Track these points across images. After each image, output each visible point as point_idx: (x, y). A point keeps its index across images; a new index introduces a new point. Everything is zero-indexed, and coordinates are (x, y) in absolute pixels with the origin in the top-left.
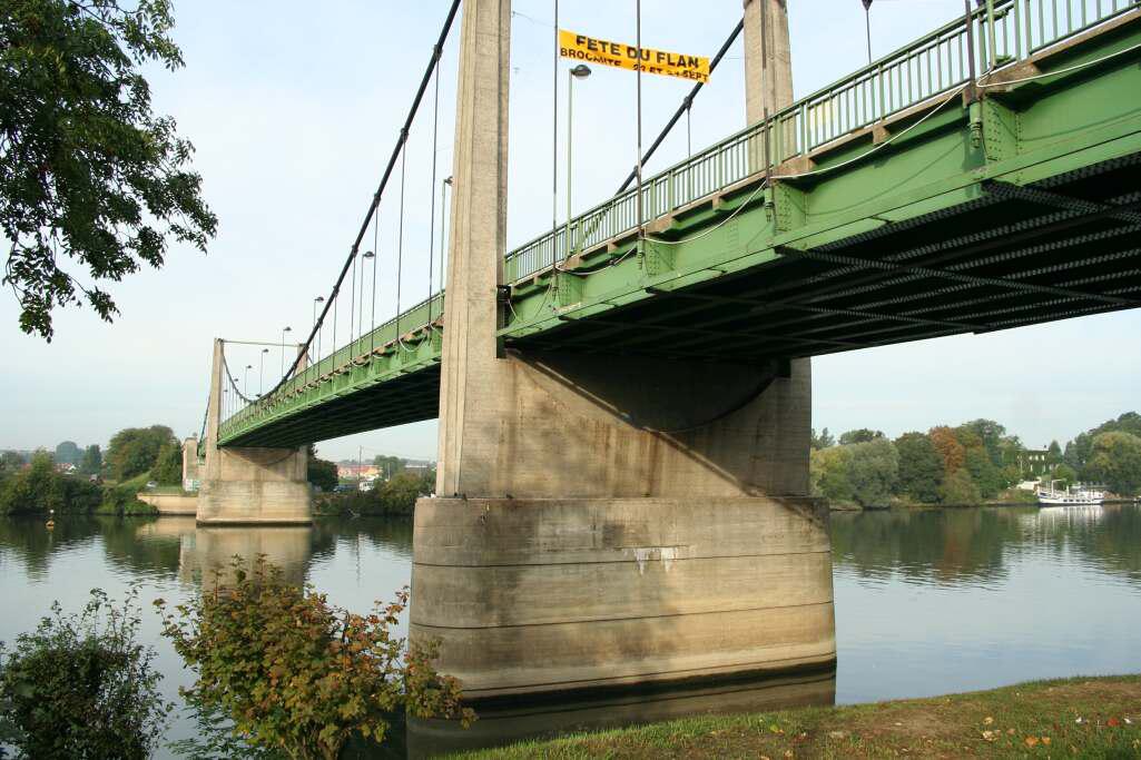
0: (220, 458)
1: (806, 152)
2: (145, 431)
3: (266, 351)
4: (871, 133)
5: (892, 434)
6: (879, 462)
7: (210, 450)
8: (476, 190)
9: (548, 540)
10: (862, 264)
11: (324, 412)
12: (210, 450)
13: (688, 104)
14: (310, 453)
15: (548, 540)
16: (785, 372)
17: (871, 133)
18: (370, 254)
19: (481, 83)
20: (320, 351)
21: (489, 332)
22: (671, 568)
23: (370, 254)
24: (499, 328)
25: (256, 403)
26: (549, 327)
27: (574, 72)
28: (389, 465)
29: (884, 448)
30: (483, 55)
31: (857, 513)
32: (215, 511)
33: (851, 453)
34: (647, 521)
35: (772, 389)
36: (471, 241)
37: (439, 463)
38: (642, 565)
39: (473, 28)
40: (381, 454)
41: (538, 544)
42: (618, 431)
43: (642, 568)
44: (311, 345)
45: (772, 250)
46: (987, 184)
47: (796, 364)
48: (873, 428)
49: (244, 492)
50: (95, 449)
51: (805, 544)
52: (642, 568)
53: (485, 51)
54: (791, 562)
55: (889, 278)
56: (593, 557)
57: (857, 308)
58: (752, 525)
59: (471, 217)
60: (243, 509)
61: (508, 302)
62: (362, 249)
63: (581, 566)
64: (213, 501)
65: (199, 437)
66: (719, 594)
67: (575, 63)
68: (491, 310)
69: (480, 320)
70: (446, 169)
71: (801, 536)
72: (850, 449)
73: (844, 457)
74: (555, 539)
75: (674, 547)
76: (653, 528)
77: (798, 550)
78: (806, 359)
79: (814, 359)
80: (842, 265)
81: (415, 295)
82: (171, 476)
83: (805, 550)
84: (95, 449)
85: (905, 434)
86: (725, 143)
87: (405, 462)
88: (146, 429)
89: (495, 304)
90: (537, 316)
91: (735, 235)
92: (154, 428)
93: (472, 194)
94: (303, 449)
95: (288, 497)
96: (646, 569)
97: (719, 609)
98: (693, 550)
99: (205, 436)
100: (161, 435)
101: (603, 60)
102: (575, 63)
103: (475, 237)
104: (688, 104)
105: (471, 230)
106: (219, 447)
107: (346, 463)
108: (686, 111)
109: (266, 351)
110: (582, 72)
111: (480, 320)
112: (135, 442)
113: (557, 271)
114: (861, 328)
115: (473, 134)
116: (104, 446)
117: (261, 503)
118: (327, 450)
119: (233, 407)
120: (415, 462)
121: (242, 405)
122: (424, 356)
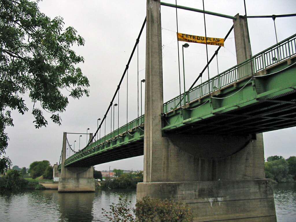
0: (65, 170)
1: (264, 68)
2: (39, 162)
3: (81, 136)
4: (287, 61)
5: (286, 157)
6: (281, 166)
7: (62, 168)
8: (153, 84)
9: (181, 196)
10: (284, 103)
11: (97, 157)
12: (62, 168)
13: (216, 53)
14: (94, 168)
15: (181, 196)
16: (254, 138)
17: (287, 61)
18: (116, 105)
19: (154, 50)
20: (102, 134)
21: (159, 127)
22: (221, 204)
23: (116, 105)
24: (162, 127)
25: (78, 152)
26: (179, 126)
27: (183, 46)
28: (118, 172)
29: (283, 161)
30: (154, 42)
31: (276, 184)
32: (64, 187)
33: (272, 164)
34: (212, 189)
35: (251, 144)
36: (152, 100)
37: (144, 172)
38: (211, 203)
39: (150, 34)
40: (115, 168)
41: (177, 197)
42: (202, 160)
43: (211, 204)
44: (97, 134)
45: (256, 100)
46: (67, 99)
47: (258, 135)
48: (279, 155)
49: (73, 181)
50: (24, 168)
51: (265, 195)
52: (211, 204)
53: (154, 40)
54: (260, 201)
55: (294, 106)
56: (195, 201)
57: (280, 116)
58: (247, 189)
59: (152, 92)
60: (73, 187)
61: (165, 119)
62: (114, 103)
63: (191, 204)
64: (63, 184)
65: (58, 164)
66: (238, 212)
67: (184, 43)
68: (159, 121)
69: (157, 125)
70: (143, 76)
71: (263, 192)
72: (271, 163)
73: (269, 165)
74: (183, 195)
75: (221, 197)
76: (214, 190)
77: (263, 197)
78: (261, 133)
79: (264, 134)
80: (278, 103)
81: (133, 117)
82: (49, 177)
83: (265, 197)
84: (24, 168)
85: (291, 157)
86: (242, 64)
87: (123, 171)
88: (41, 162)
89: (161, 120)
90: (177, 122)
91: (242, 95)
92: (44, 161)
93: (152, 85)
94: (92, 167)
95: (87, 183)
96: (213, 204)
97: (238, 218)
98: (228, 198)
99: (60, 163)
100: (46, 163)
101: (191, 41)
102: (184, 43)
103: (154, 98)
104: (216, 53)
105: (152, 96)
106: (65, 167)
107: (103, 171)
108: (216, 55)
109: (81, 136)
110: (186, 46)
111: (157, 125)
112: (37, 166)
113: (182, 108)
114: (282, 122)
115: (152, 66)
116: (28, 167)
117: (79, 185)
118: (98, 168)
119: (69, 154)
120: (126, 171)
121: (72, 154)
122: (137, 137)
